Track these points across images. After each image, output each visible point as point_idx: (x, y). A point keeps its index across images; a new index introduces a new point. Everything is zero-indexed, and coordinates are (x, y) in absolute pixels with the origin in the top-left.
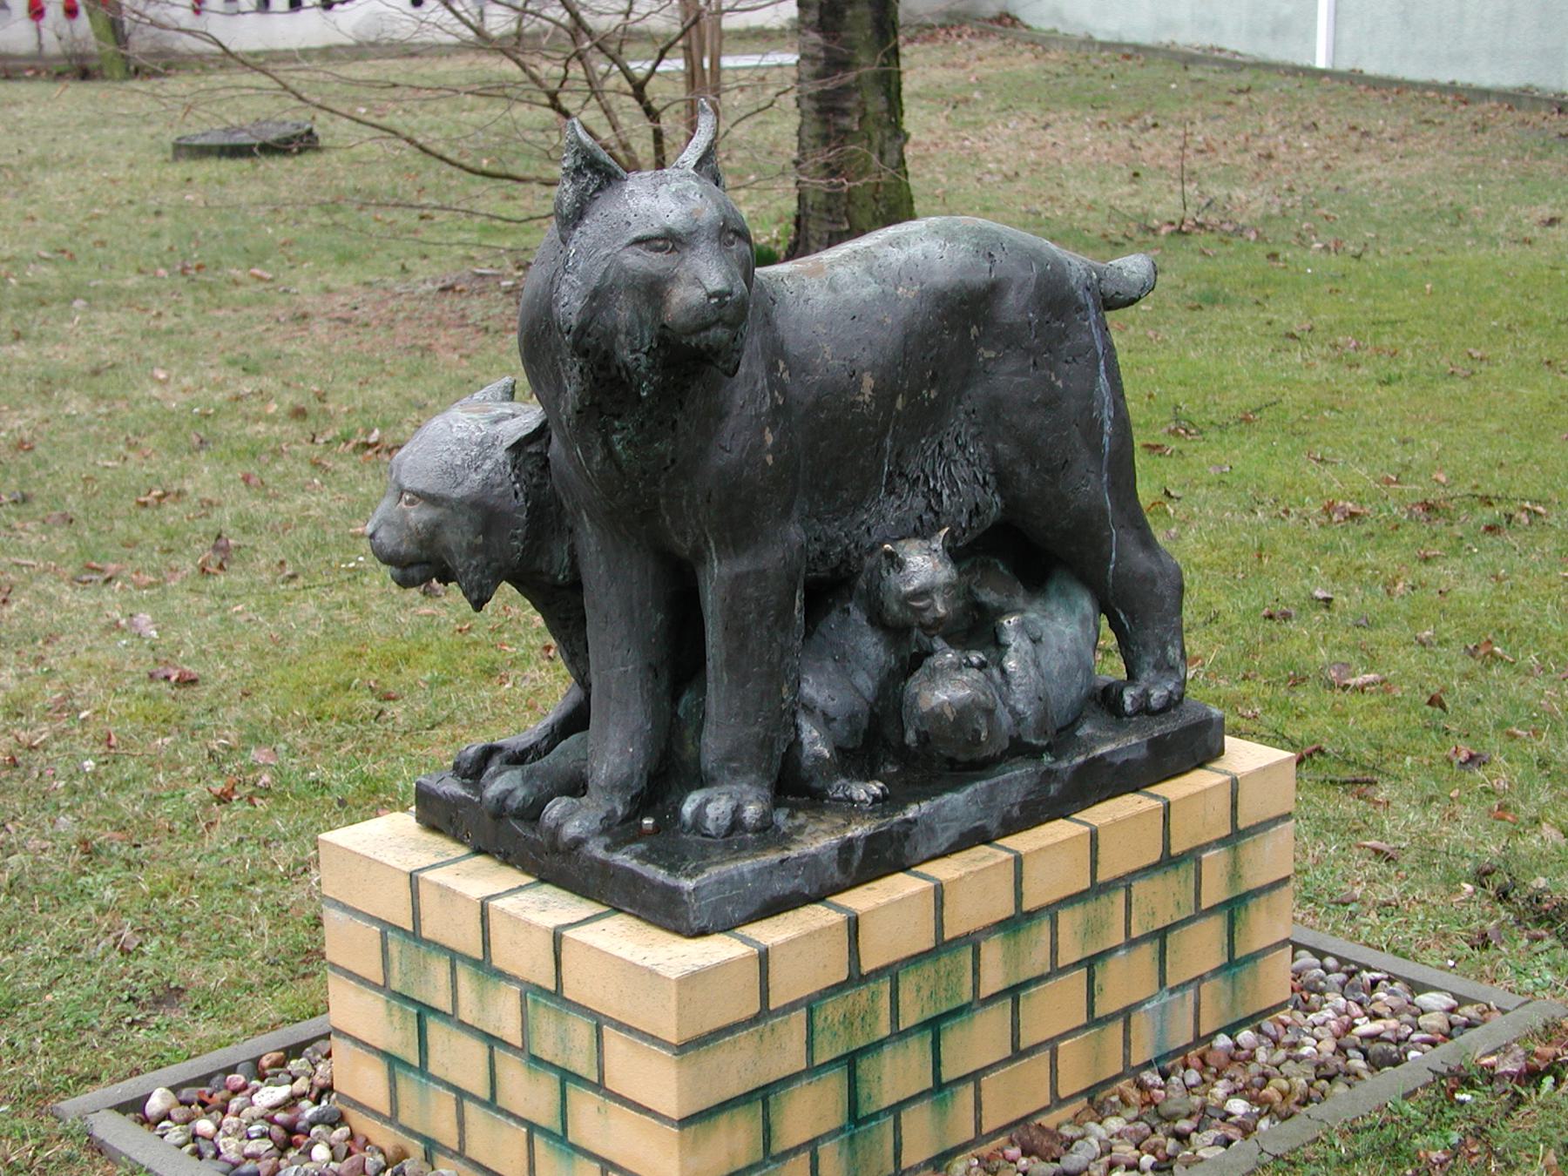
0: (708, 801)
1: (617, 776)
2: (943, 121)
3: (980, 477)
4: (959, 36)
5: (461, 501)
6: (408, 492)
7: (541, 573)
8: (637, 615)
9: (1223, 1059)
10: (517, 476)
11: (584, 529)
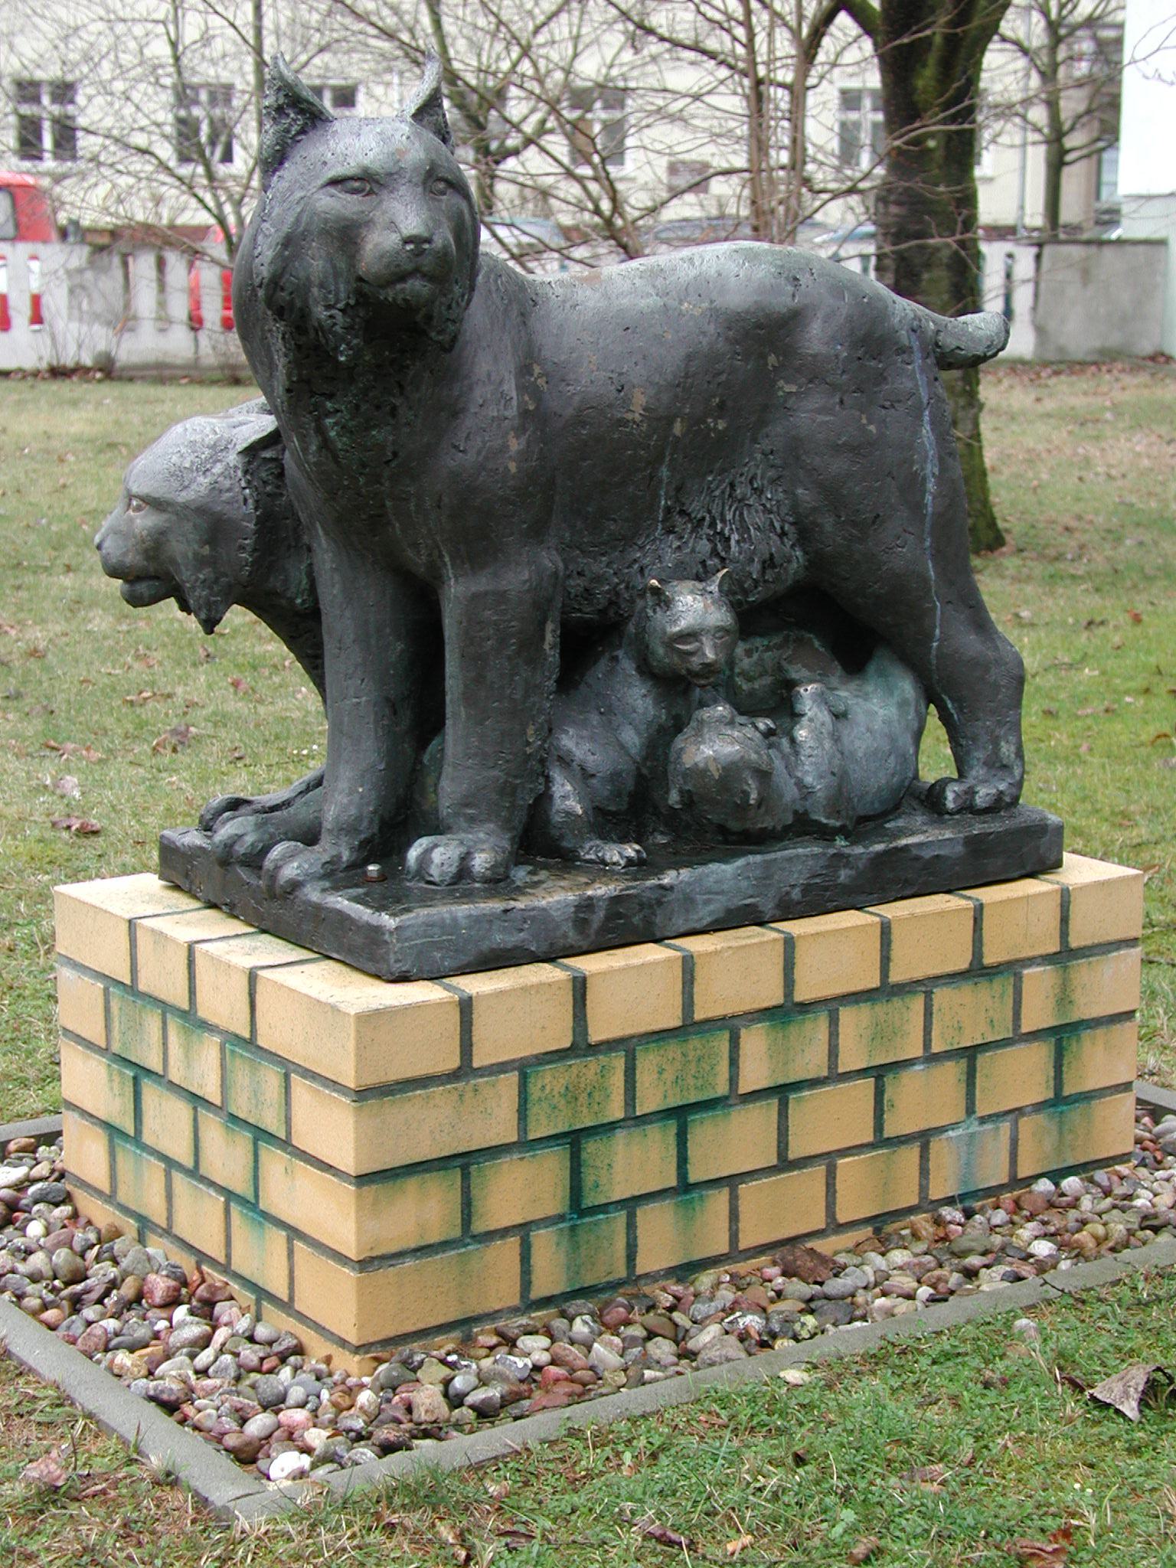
0: (436, 846)
1: (344, 818)
2: (1065, 434)
3: (777, 525)
4: (1109, 371)
5: (185, 506)
6: (137, 497)
7: (276, 594)
8: (373, 642)
9: (1040, 1203)
10: (249, 482)
11: (320, 545)
